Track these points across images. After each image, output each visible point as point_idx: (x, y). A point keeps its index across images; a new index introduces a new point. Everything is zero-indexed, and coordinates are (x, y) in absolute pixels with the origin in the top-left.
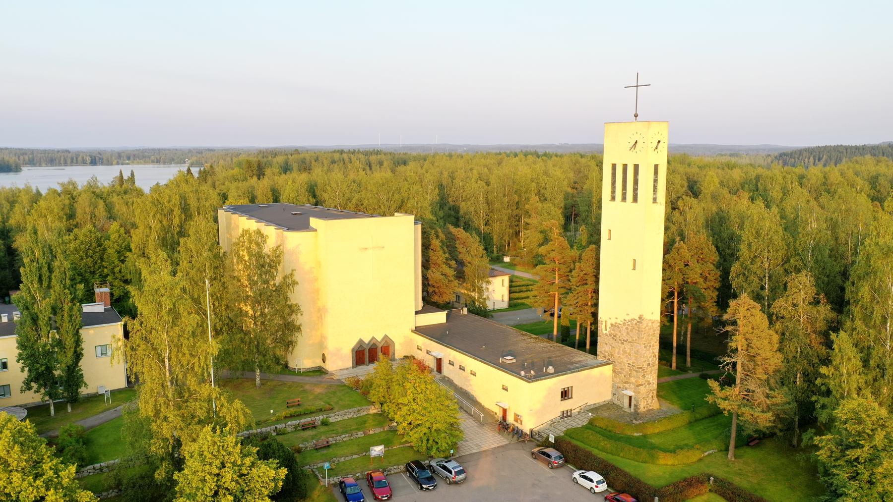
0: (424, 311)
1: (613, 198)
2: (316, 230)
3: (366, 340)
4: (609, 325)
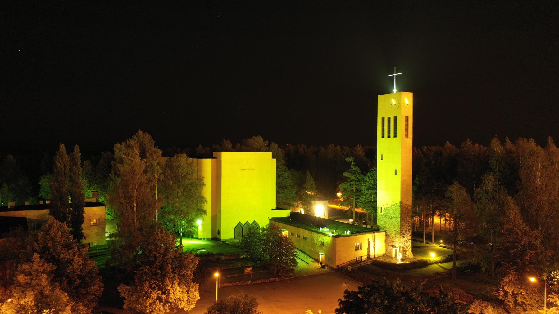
0: (278, 209)
1: (383, 137)
2: (216, 158)
3: (243, 223)
4: (383, 209)
